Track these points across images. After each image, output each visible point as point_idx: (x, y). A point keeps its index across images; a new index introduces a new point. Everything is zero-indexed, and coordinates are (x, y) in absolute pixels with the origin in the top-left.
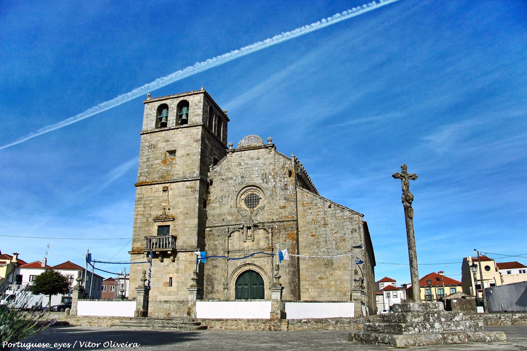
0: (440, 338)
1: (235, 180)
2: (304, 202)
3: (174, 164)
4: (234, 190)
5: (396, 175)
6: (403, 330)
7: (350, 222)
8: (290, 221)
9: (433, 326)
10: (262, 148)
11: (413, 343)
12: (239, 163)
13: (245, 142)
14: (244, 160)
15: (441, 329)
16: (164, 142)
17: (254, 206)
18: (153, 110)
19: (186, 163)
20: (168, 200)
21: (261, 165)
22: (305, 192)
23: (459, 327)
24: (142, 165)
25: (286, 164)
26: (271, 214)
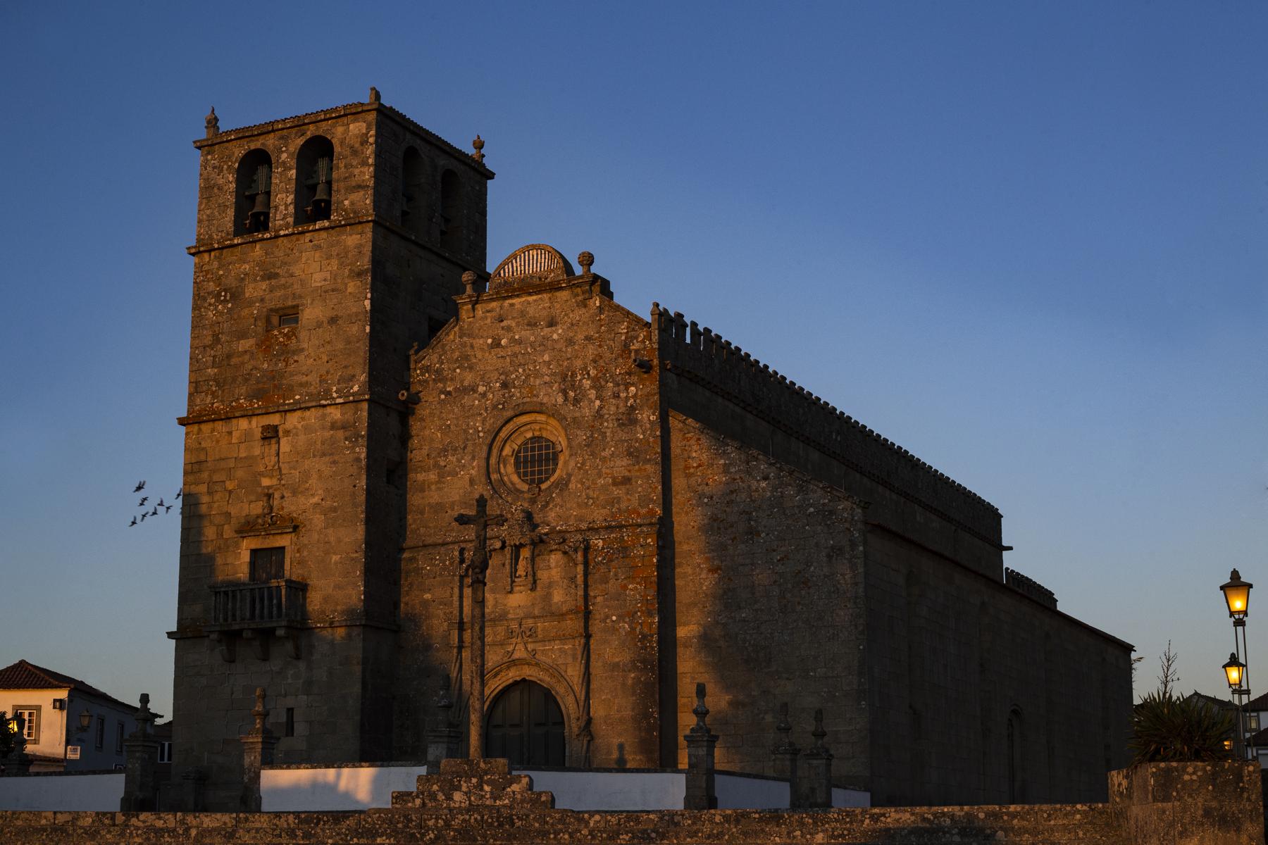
1: (484, 395)
2: (690, 461)
3: (295, 352)
4: (480, 429)
7: (826, 524)
8: (640, 526)
10: (561, 289)
12: (494, 339)
13: (515, 269)
14: (509, 329)
16: (263, 279)
18: (225, 172)
19: (328, 347)
20: (276, 467)
24: (200, 357)
26: (586, 503)
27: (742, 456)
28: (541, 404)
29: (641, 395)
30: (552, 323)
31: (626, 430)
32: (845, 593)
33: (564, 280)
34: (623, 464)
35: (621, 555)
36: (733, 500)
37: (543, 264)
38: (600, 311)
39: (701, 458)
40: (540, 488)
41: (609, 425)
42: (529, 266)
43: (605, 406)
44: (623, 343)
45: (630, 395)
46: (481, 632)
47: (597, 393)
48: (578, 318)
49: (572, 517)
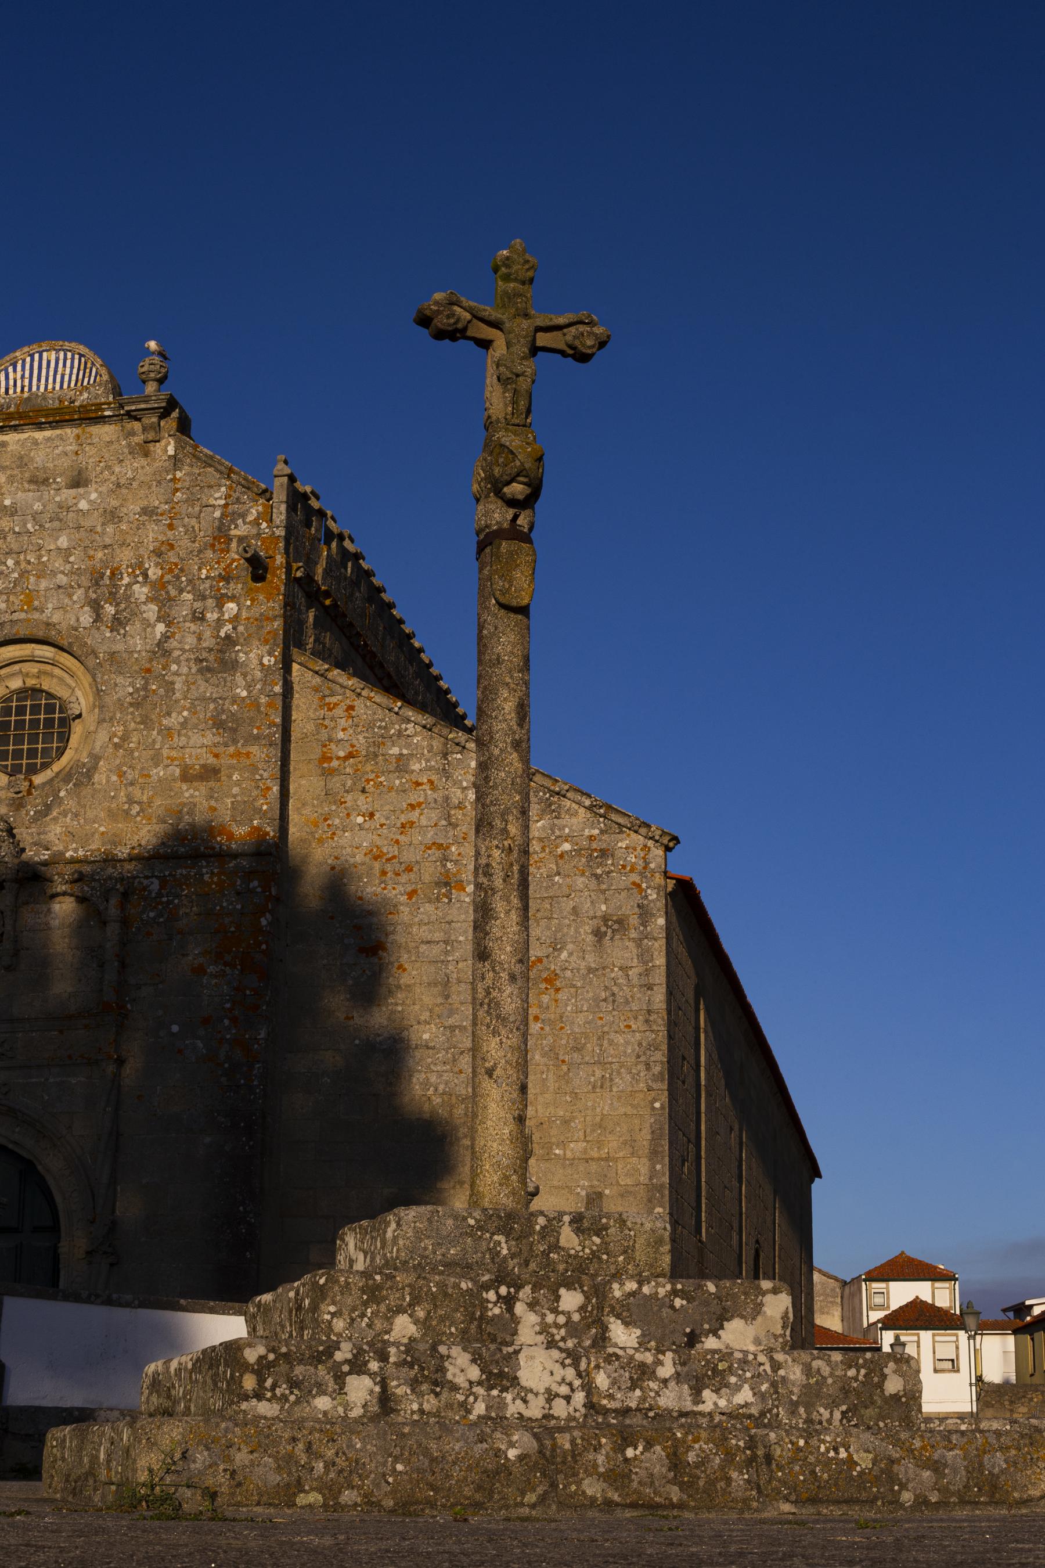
0: (512, 1454)
5: (438, 312)
6: (249, 1382)
9: (501, 1375)
10: (102, 420)
11: (274, 1479)
13: (11, 382)
15: (568, 1399)
17: (39, 761)
21: (95, 520)
22: (342, 691)
23: (717, 1391)
25: (235, 516)
26: (127, 812)
27: (435, 743)
28: (48, 624)
29: (248, 619)
30: (78, 481)
31: (214, 680)
32: (627, 1002)
33: (109, 404)
34: (205, 742)
35: (195, 909)
36: (413, 823)
37: (66, 378)
38: (175, 465)
39: (355, 742)
40: (31, 781)
41: (180, 671)
42: (39, 380)
43: (174, 633)
44: (217, 523)
45: (226, 617)
46: (520, 725)
47: (159, 612)
48: (130, 475)
49: (97, 836)
